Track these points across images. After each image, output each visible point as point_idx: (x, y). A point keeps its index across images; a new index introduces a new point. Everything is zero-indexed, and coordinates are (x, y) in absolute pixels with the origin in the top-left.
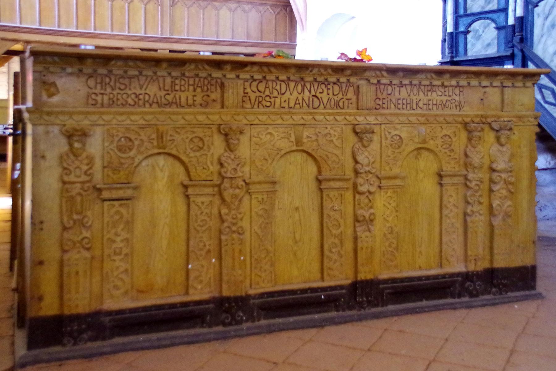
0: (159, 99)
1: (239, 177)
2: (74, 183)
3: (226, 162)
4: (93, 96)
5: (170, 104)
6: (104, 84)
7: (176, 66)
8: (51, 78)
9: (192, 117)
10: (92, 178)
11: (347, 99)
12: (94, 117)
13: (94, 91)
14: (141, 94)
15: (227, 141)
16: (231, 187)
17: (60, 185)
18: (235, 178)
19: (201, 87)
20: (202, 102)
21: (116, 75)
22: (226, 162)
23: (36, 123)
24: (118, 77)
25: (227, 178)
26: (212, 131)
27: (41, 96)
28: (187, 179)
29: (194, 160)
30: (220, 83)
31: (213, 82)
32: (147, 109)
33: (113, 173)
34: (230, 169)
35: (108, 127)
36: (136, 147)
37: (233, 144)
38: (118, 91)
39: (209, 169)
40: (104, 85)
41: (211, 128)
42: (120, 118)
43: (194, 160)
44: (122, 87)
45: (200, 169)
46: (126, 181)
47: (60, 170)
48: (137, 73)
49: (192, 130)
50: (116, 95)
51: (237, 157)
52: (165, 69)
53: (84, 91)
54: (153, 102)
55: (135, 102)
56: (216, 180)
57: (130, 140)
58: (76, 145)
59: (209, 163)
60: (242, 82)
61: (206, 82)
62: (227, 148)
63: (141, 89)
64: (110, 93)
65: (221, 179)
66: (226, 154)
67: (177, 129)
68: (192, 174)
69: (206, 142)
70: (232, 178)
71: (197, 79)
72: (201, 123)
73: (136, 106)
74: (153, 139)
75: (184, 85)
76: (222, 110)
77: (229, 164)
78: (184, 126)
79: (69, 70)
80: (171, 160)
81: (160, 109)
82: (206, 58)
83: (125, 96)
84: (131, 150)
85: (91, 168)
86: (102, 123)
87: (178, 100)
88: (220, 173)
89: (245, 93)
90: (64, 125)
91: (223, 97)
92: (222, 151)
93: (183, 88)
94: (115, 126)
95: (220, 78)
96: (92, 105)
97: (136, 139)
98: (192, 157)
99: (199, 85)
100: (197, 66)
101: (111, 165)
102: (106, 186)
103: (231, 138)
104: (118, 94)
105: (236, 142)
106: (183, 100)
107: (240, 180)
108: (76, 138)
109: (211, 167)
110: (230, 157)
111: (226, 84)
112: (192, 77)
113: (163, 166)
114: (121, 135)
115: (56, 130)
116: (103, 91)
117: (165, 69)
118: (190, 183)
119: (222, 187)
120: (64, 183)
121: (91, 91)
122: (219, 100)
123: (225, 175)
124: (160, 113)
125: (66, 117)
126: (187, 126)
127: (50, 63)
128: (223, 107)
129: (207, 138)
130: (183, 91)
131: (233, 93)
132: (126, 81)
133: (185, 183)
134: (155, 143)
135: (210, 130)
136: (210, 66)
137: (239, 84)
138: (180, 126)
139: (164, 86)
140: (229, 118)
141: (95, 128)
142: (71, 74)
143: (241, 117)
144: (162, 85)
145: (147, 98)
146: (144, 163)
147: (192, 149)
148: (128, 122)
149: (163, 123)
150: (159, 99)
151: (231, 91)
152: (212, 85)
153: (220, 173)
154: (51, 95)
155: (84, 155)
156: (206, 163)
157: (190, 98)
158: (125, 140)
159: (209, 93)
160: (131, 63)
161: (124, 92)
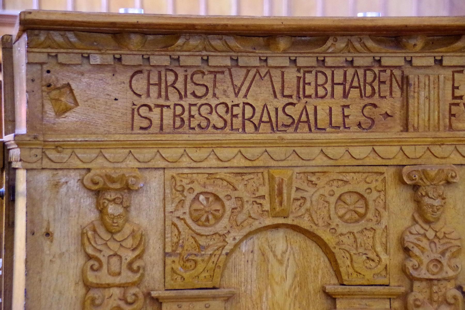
0: (273, 114)
1: (448, 280)
2: (109, 286)
3: (418, 246)
4: (144, 111)
5: (295, 124)
6: (163, 85)
7: (307, 44)
8: (61, 77)
9: (342, 150)
10: (143, 275)
12: (147, 154)
13: (144, 100)
14: (237, 105)
15: (418, 202)
16: (431, 300)
17: (82, 291)
18: (438, 280)
19: (359, 87)
20: (362, 119)
21: (186, 67)
22: (418, 246)
23: (34, 166)
24: (189, 73)
25: (421, 280)
26: (384, 180)
27: (43, 112)
28: (334, 280)
29: (347, 241)
30: (399, 79)
31: (385, 76)
32: (250, 135)
33: (184, 267)
34: (425, 261)
35: (173, 172)
36: (228, 212)
37: (432, 206)
38: (193, 100)
39: (380, 261)
40: (163, 89)
41: (382, 174)
42: (196, 154)
43: (347, 241)
44: (200, 91)
45: (360, 260)
46: (210, 284)
47: (81, 260)
48: (228, 62)
49: (341, 177)
50: (187, 107)
51: (440, 235)
52: (285, 51)
53: (126, 100)
54: (261, 121)
55: (225, 122)
56: (397, 285)
57: (217, 198)
58: (111, 209)
59: (379, 249)
60: (449, 73)
61: (370, 77)
62: (416, 216)
63: (236, 95)
64: (176, 105)
65: (407, 281)
66: (417, 229)
67: (310, 176)
68: (343, 270)
69: (371, 203)
70: (431, 280)
71: (350, 72)
72: (360, 162)
73: (228, 129)
74: (263, 197)
75: (322, 85)
76: (405, 135)
77: (423, 250)
78: (325, 169)
79: (96, 59)
80: (298, 240)
81: (276, 135)
82: (370, 24)
83: (205, 110)
84: (218, 219)
85: (139, 257)
86: (163, 164)
87: (312, 117)
88: (404, 270)
89: (454, 97)
90: (89, 170)
91: (406, 106)
92: (408, 222)
93: (321, 92)
94: (186, 171)
95: (399, 67)
96: (141, 128)
97: (228, 197)
98: (341, 234)
99: (355, 84)
100: (349, 43)
101: (179, 250)
102: (168, 293)
103: (427, 195)
104: (190, 105)
105: (437, 203)
106: (322, 115)
107: (450, 285)
108: (111, 196)
109: (384, 257)
110: (425, 236)
111: (413, 79)
112: (339, 67)
113: (284, 253)
114: (198, 189)
115: (72, 181)
116: (161, 101)
117: (285, 51)
118: (340, 289)
119: (411, 299)
120: (88, 287)
121: (139, 102)
122: (398, 114)
123: (415, 274)
124: (274, 143)
125: (93, 153)
126: (330, 169)
127: (60, 46)
128: (406, 129)
129: (375, 194)
130: (322, 97)
131: (428, 98)
132: (208, 80)
133: (329, 289)
134: (267, 207)
135: (380, 178)
136: (379, 42)
137: (442, 78)
138: (316, 169)
139: (365, 94)
140: (420, 151)
141: (147, 174)
142: (101, 67)
143: (448, 150)
144: (278, 87)
145: (248, 112)
146: (244, 248)
147: (341, 217)
148: (213, 162)
149: (281, 164)
150: (273, 114)
151: (423, 94)
152: (381, 82)
153: (404, 270)
154: (62, 111)
155: (127, 229)
156: (373, 247)
157: (337, 111)
158: (207, 199)
159: (376, 100)
160: (217, 43)
161: (203, 101)
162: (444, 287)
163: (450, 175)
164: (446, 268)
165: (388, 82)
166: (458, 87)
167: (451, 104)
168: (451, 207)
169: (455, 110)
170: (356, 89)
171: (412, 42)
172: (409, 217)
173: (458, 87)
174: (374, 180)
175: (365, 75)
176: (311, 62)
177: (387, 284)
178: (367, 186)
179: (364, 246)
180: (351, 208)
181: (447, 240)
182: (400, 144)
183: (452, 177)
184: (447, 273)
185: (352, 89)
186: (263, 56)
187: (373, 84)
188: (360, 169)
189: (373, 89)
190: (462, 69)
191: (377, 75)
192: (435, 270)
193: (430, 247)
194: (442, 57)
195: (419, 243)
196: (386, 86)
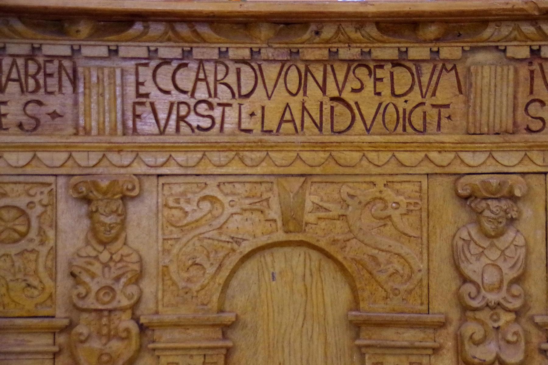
3: (88, 271)
11: (433, 106)
19: (18, 80)
31: (52, 68)
41: (49, 184)
59: (43, 274)
61: (32, 68)
70: (101, 310)
72: (20, 171)
77: (93, 276)
89: (139, 95)
92: (80, 243)
99: (14, 75)
129: (39, 209)
135: (46, 190)
152: (48, 75)
156: (36, 272)
159: (40, 96)
162: (118, 319)
163: (125, 187)
164: (119, 296)
165: (56, 75)
166: (144, 83)
167: (135, 104)
168: (135, 224)
169: (139, 109)
170: (15, 83)
171: (74, 28)
172: (82, 237)
173: (144, 83)
174: (38, 193)
175: (26, 66)
176: (245, 53)
177: (52, 315)
178: (28, 200)
179: (25, 270)
180: (10, 225)
181: (124, 264)
182: (69, 150)
183: (128, 189)
184: (119, 302)
185: (10, 83)
186: (152, 46)
187: (38, 77)
188: (21, 179)
189: (37, 82)
190: (147, 61)
191: (42, 66)
192: (107, 299)
193: (103, 272)
194: (41, 45)
195: (89, 267)
196: (53, 79)
